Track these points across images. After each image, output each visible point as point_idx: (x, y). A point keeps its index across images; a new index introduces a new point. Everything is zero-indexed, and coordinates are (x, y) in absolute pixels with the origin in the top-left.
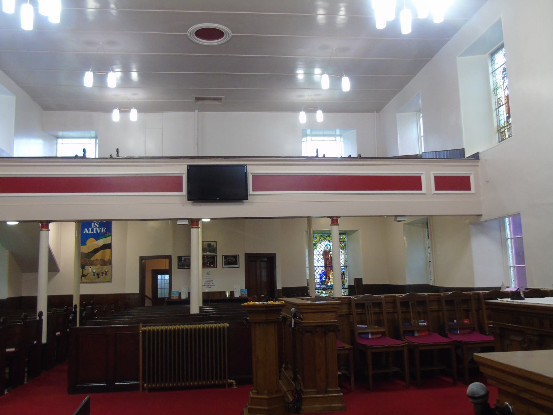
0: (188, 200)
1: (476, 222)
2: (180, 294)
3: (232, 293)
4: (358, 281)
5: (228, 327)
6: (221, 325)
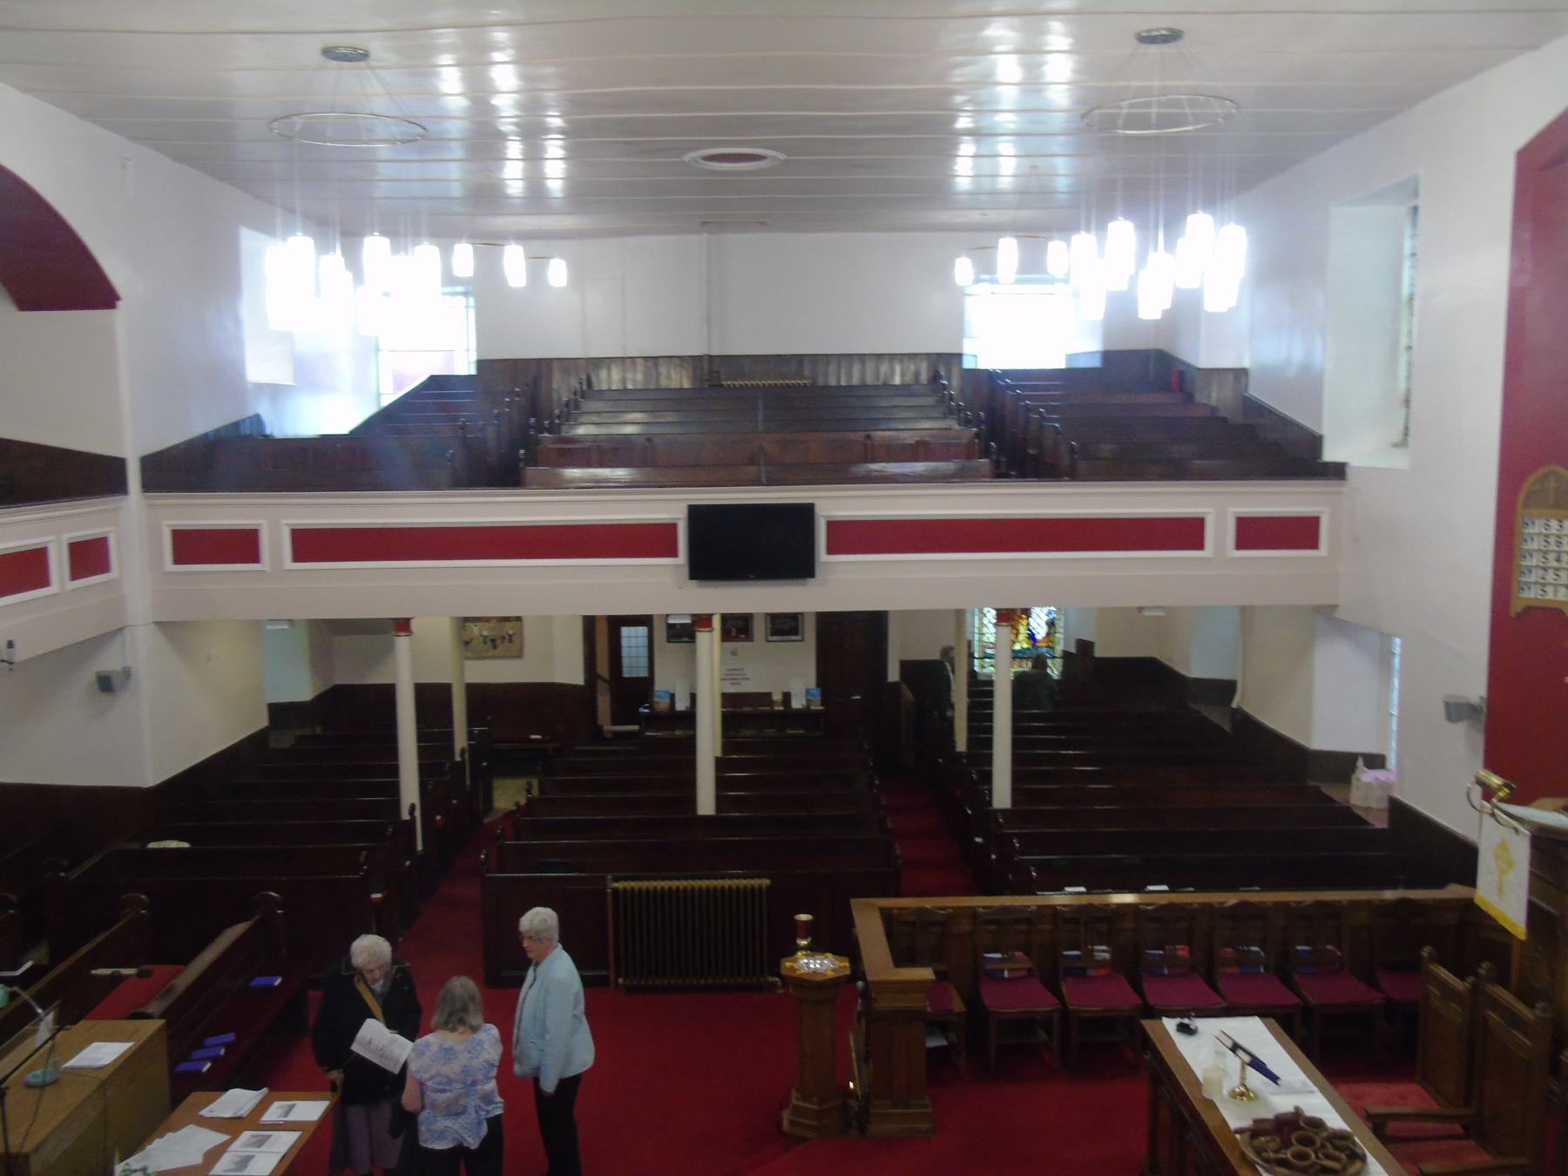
0: (692, 577)
1: (1325, 618)
2: (672, 697)
3: (787, 697)
4: (1085, 647)
5: (769, 888)
6: (755, 882)
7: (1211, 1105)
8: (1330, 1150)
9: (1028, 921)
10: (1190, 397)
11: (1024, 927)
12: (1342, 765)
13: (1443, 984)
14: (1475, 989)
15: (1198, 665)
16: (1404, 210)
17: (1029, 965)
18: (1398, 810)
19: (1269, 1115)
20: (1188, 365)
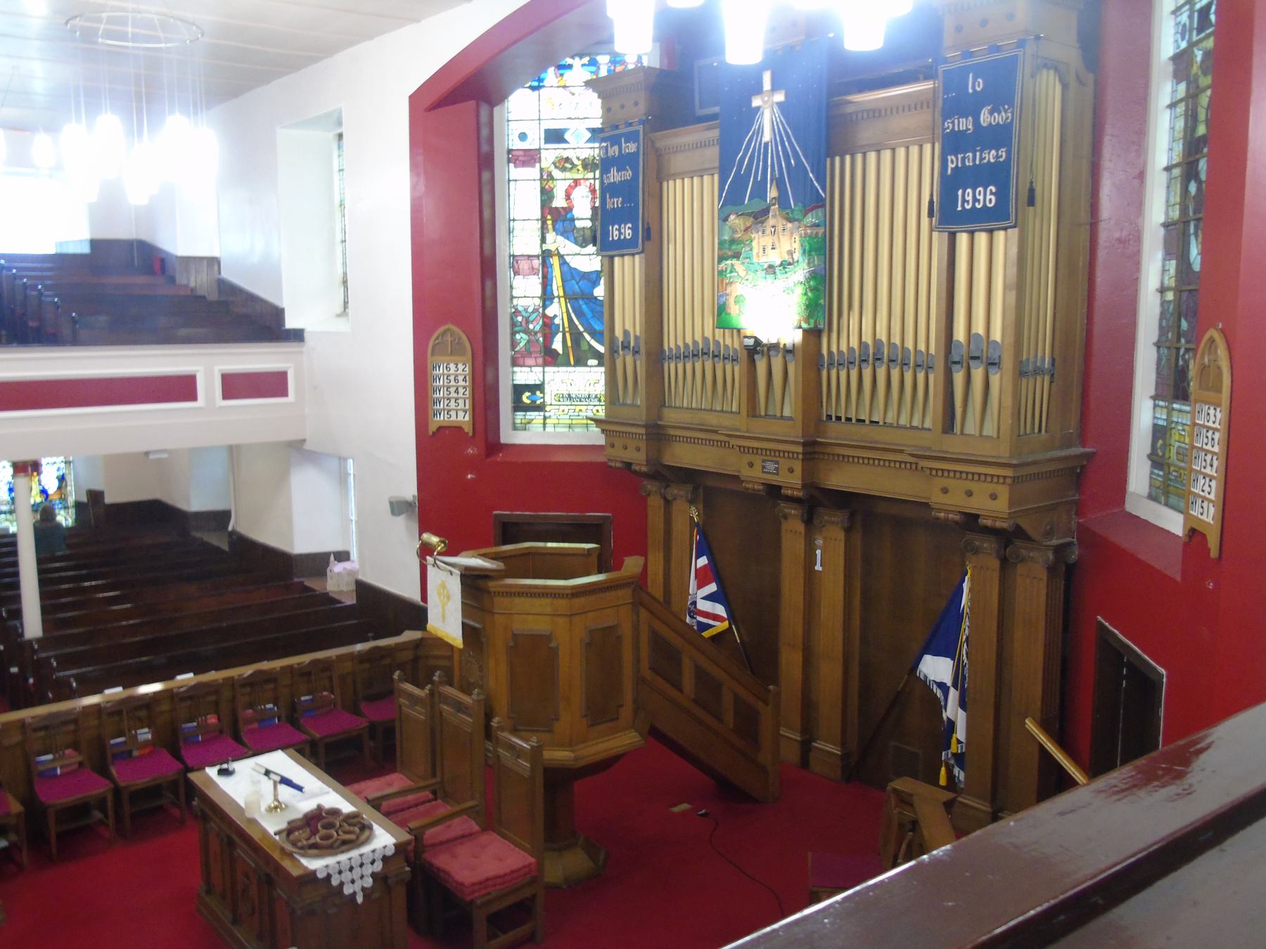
1: (296, 450)
7: (253, 822)
8: (347, 827)
9: (75, 721)
10: (172, 280)
11: (72, 727)
12: (318, 563)
13: (410, 696)
14: (432, 693)
15: (196, 501)
16: (331, 135)
17: (79, 759)
18: (363, 589)
19: (300, 816)
20: (167, 253)
